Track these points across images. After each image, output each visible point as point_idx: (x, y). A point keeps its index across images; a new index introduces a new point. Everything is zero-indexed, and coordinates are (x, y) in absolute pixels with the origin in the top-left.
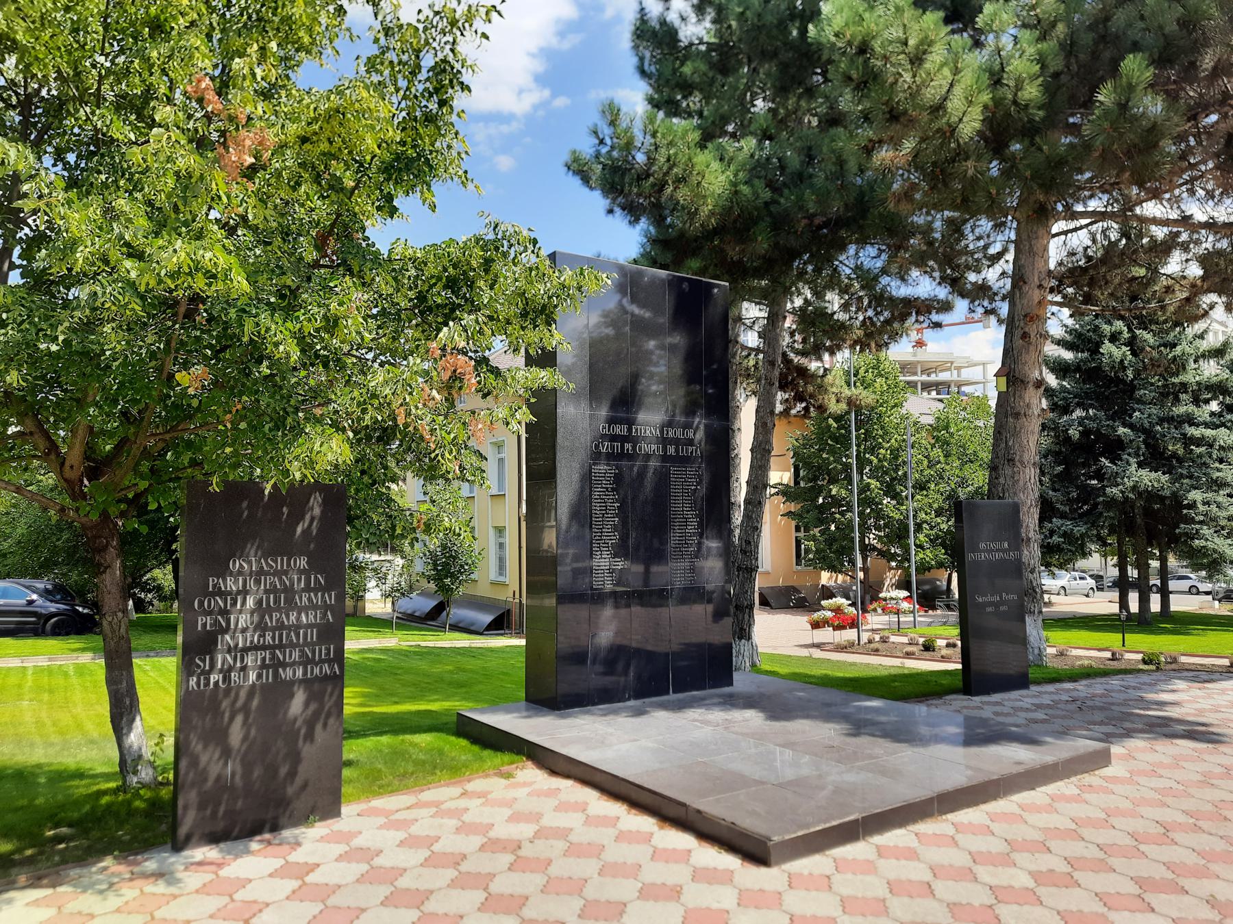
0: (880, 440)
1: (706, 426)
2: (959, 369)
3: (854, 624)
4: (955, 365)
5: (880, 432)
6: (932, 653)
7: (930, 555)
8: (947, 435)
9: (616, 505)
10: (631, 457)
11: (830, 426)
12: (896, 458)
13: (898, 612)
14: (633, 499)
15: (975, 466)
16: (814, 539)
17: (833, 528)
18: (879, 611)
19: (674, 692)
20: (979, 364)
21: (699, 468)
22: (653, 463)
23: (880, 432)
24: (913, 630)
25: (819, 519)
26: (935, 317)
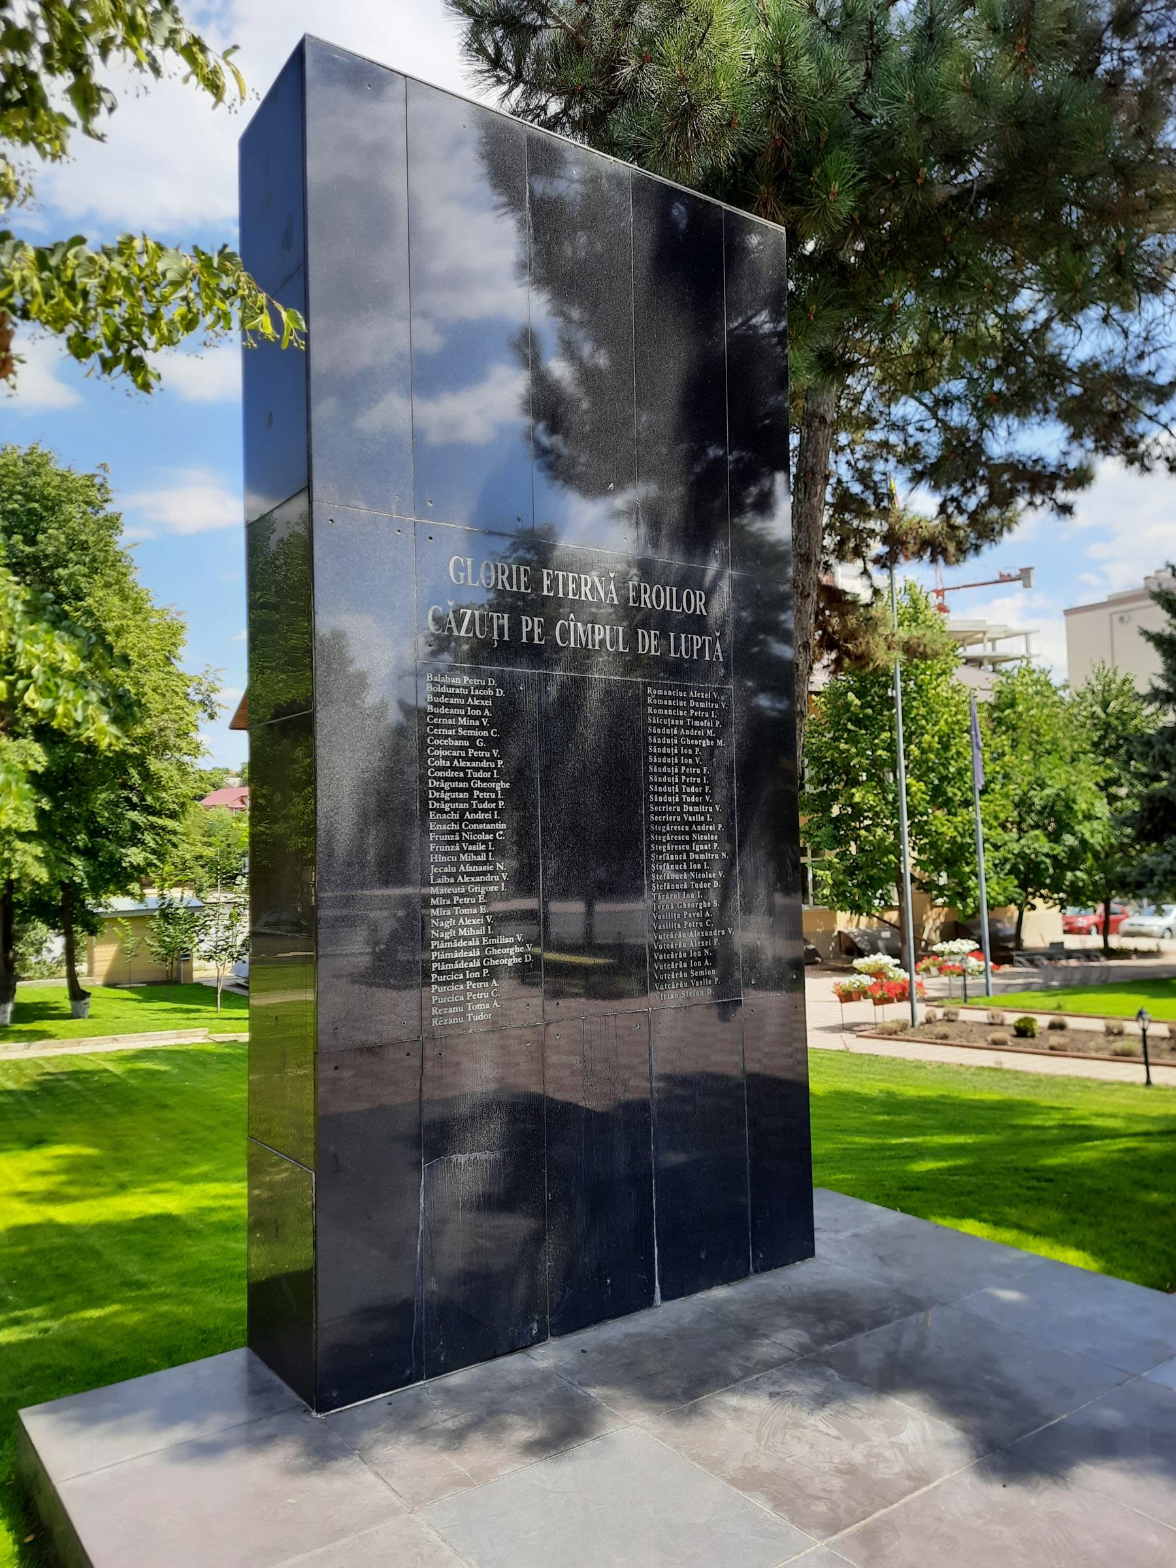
0: (923, 722)
1: (735, 584)
2: (993, 641)
3: (904, 994)
4: (988, 635)
5: (923, 711)
6: (1030, 1040)
7: (996, 888)
8: (1012, 716)
9: (499, 786)
10: (539, 654)
11: (848, 705)
12: (946, 747)
13: (963, 973)
14: (547, 770)
15: (1054, 758)
16: (830, 866)
17: (853, 849)
18: (934, 971)
19: (665, 1298)
20: (1019, 634)
21: (720, 691)
22: (601, 674)
23: (923, 711)
24: (986, 999)
25: (834, 837)
26: (1062, 496)
